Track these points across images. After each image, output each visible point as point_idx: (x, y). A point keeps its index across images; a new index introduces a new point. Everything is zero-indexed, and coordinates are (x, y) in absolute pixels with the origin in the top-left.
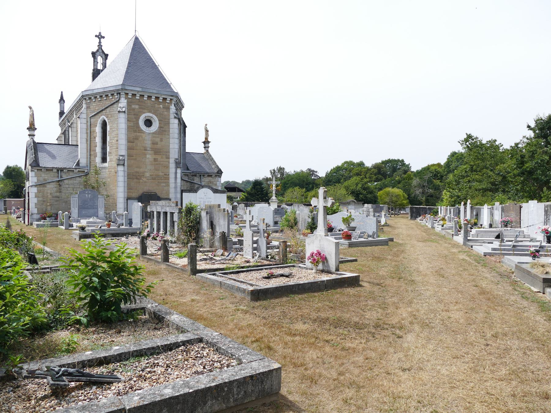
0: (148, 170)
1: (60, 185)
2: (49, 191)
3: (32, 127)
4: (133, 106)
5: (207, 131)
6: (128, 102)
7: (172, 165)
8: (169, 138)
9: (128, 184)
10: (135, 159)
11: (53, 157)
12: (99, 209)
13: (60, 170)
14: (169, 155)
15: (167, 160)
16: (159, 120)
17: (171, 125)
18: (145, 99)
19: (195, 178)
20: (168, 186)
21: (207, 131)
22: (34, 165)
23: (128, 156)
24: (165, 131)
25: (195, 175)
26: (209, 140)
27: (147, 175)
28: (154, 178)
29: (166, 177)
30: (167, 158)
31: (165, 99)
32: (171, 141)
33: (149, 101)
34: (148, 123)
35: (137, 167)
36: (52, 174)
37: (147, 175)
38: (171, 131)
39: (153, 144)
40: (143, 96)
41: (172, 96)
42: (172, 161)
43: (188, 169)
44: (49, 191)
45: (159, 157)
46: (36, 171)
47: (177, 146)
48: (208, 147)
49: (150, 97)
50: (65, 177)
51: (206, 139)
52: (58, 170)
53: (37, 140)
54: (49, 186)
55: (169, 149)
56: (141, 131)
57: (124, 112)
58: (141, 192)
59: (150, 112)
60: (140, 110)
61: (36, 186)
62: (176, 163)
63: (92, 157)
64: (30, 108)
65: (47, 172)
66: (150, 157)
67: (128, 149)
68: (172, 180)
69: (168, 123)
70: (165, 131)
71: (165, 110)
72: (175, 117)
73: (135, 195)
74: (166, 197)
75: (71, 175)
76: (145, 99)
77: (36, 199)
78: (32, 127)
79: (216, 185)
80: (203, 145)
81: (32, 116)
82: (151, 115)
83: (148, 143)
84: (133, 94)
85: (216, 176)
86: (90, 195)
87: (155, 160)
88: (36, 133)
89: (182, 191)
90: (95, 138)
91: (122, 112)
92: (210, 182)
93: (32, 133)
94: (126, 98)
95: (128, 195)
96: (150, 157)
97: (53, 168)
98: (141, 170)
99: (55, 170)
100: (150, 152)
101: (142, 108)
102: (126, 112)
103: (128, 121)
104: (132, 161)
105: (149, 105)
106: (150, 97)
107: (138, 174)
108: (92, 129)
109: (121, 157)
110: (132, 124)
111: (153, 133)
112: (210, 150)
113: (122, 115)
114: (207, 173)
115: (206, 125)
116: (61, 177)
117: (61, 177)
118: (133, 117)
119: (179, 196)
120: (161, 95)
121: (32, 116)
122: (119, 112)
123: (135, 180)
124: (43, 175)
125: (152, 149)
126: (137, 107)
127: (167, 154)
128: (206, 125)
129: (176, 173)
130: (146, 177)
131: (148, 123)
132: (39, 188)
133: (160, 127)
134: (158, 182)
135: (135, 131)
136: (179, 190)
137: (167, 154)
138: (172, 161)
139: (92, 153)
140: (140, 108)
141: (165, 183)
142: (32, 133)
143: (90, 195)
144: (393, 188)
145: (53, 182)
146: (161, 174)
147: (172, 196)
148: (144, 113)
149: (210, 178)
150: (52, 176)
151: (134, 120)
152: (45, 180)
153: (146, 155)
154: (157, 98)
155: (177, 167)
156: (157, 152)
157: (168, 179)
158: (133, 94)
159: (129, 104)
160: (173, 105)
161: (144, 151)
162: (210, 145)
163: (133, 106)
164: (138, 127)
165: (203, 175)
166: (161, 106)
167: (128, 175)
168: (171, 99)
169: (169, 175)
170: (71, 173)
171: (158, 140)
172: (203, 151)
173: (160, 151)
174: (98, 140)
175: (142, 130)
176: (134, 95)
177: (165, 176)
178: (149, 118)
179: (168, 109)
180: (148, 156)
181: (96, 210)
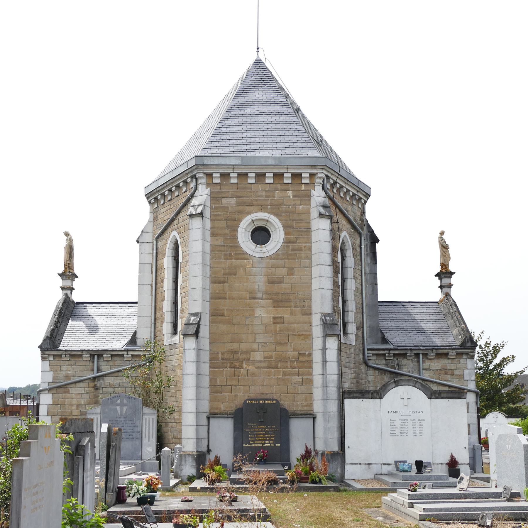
0: (258, 344)
1: (96, 388)
2: (75, 402)
3: (68, 274)
4: (224, 201)
5: (444, 247)
6: (212, 193)
7: (317, 331)
8: (310, 266)
9: (210, 380)
10: (229, 322)
11: (93, 328)
12: (145, 441)
13: (97, 355)
14: (310, 307)
15: (306, 318)
16: (284, 227)
17: (313, 234)
18: (252, 181)
19: (405, 362)
20: (310, 381)
21: (444, 247)
22: (47, 346)
23: (212, 314)
24: (300, 250)
25: (404, 356)
26: (451, 268)
27: (258, 356)
28: (273, 364)
29: (305, 360)
30: (305, 314)
31: (297, 176)
32: (315, 271)
33: (260, 186)
34: (261, 235)
35: (233, 340)
36: (81, 364)
37: (258, 356)
38: (315, 248)
39: (271, 282)
40: (246, 174)
41: (313, 166)
42: (316, 320)
43: (384, 340)
44: (75, 402)
45: (285, 313)
46: (51, 358)
47: (328, 284)
48: (450, 286)
49: (261, 176)
50: (106, 369)
51: (444, 266)
52: (92, 356)
53: (76, 297)
54: (74, 390)
55: (310, 292)
56: (242, 255)
57: (201, 215)
58: (240, 399)
59: (263, 209)
60: (241, 207)
61: (50, 390)
62: (325, 324)
63: (158, 324)
64: (67, 234)
65: (73, 361)
66: (263, 313)
67: (212, 298)
68: (317, 368)
69: (308, 231)
70: (300, 250)
71: (299, 202)
72: (321, 215)
73: (229, 406)
74: (305, 410)
75: (120, 365)
76: (252, 181)
77: (49, 417)
78: (68, 274)
79: (461, 377)
80: (437, 282)
81: (70, 250)
82: (264, 215)
83: (259, 283)
84: (222, 175)
85: (459, 355)
86: (125, 408)
87: (276, 320)
88: (76, 284)
89: (345, 394)
90: (162, 282)
91: (196, 215)
92: (445, 371)
93: (68, 283)
94: (207, 186)
95: (211, 407)
96: (263, 313)
97: (82, 351)
98: (243, 346)
99: (86, 356)
100: (263, 302)
101: (244, 203)
102: (207, 214)
103: (213, 234)
104: (222, 327)
105: (261, 193)
106: (261, 176)
107: (234, 356)
108: (159, 262)
109: (193, 318)
110: (220, 241)
111: (271, 258)
112: (454, 293)
113: (197, 223)
114: (434, 348)
115: (442, 233)
116: (99, 370)
117: (99, 370)
118: (224, 224)
119: (333, 407)
120: (288, 166)
121: (70, 250)
122: (191, 216)
123: (229, 371)
124: (64, 368)
125: (269, 295)
126: (233, 201)
127: (306, 304)
128: (442, 233)
129: (324, 349)
130: (254, 363)
131: (261, 235)
132: (56, 395)
133: (287, 242)
134: (285, 374)
135: (228, 257)
136: (333, 391)
137: (306, 304)
138: (316, 320)
139: (158, 315)
140: (239, 203)
141: (301, 375)
142: (68, 283)
143: (125, 408)
144: (95, 447)
145: (83, 381)
146: (291, 353)
147: (317, 408)
148: (250, 213)
149: (444, 361)
150: (82, 368)
151: (227, 231)
152: (67, 377)
153: (253, 309)
154: (279, 176)
155: (326, 336)
156: (279, 300)
157: (310, 364)
158: (222, 175)
159: (215, 197)
160: (319, 188)
161: (248, 301)
162: (454, 280)
163: (224, 201)
164: (235, 245)
165: (425, 355)
166: (290, 193)
167: (211, 359)
168: (312, 176)
169: (310, 355)
170: (118, 361)
171: (282, 272)
172: (437, 295)
173: (288, 299)
174: (167, 285)
175: (245, 253)
176: (225, 176)
177: (301, 359)
178: (263, 224)
179: (307, 197)
180: (259, 312)
181: (138, 443)
